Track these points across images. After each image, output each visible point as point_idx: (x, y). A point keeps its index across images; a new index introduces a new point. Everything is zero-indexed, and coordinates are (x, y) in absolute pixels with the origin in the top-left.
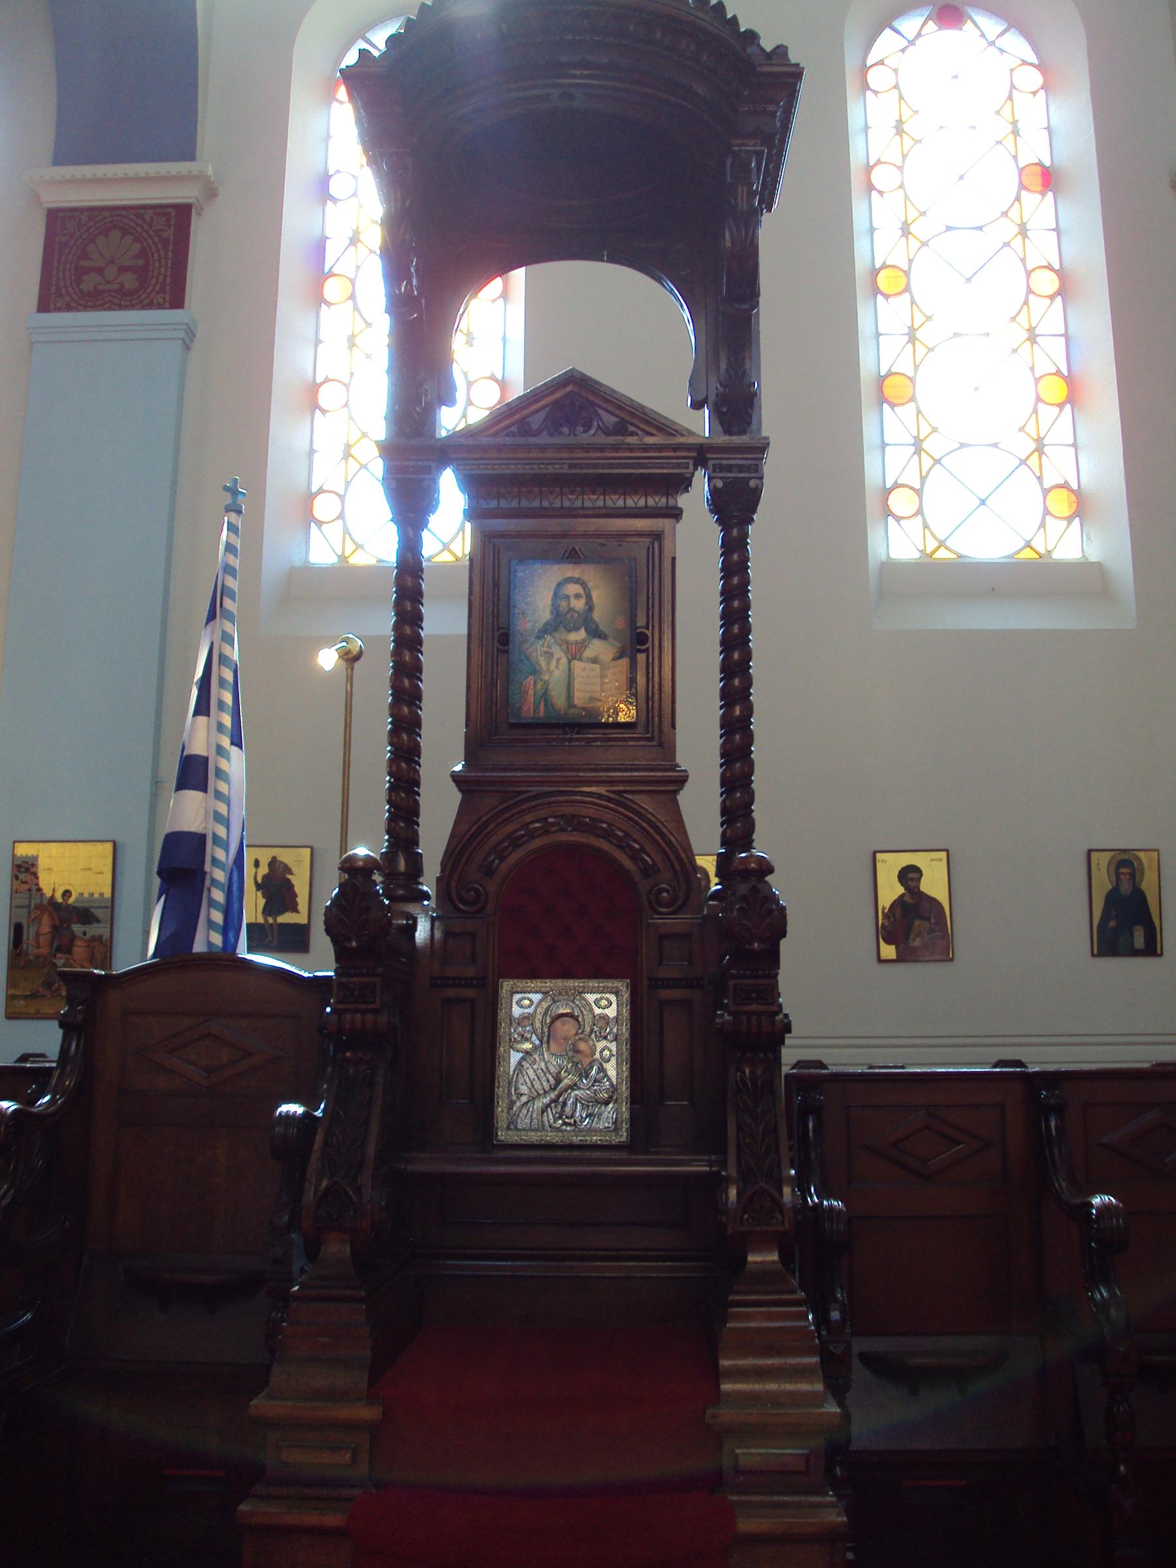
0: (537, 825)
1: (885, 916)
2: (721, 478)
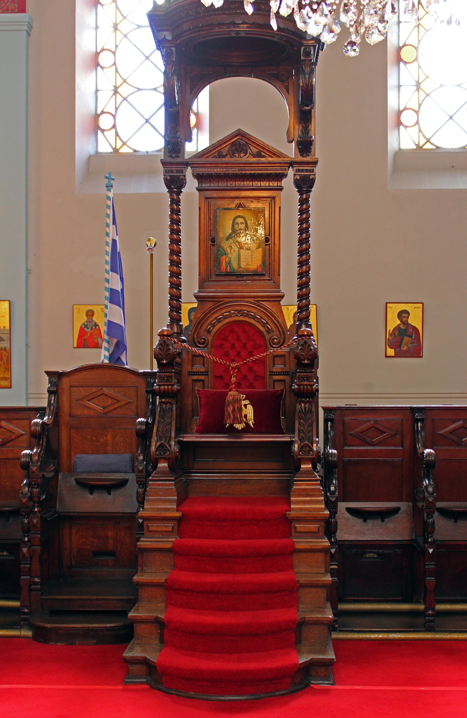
0: (227, 314)
1: (390, 335)
2: (299, 175)
